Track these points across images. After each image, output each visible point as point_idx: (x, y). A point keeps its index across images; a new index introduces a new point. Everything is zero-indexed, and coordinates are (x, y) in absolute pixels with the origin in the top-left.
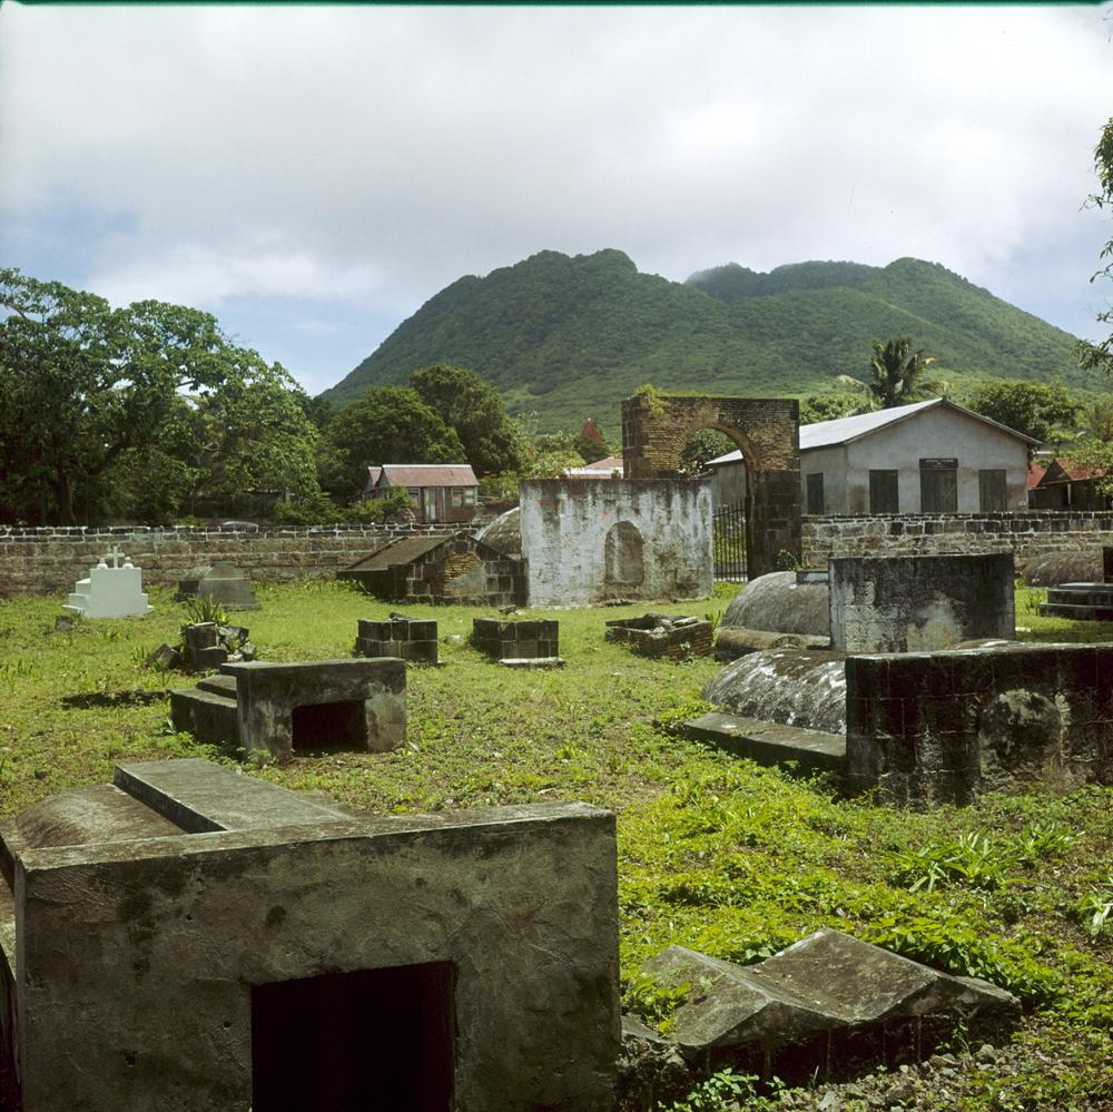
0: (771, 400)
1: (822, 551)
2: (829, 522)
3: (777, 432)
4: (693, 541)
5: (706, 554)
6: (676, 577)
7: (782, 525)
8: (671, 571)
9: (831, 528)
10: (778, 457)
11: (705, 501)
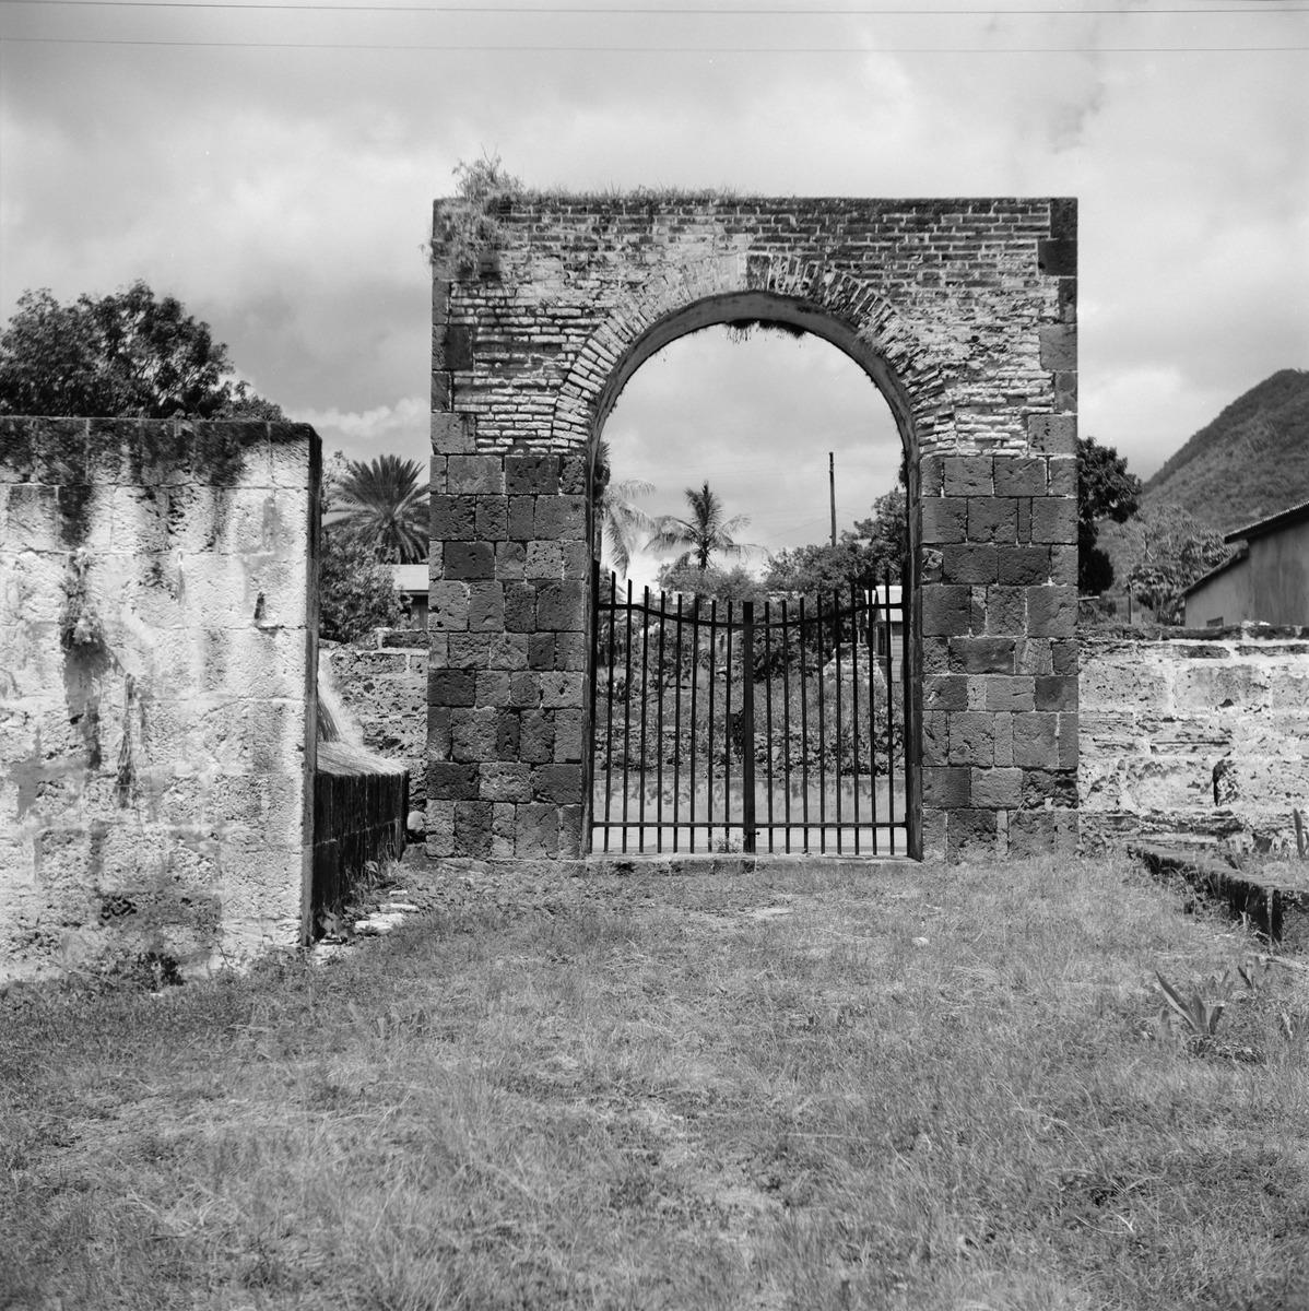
0: (961, 205)
1: (1184, 757)
2: (1221, 653)
3: (984, 318)
4: (194, 702)
5: (264, 764)
6: (96, 866)
7: (999, 658)
8: (71, 837)
9: (1226, 676)
10: (985, 408)
11: (272, 515)
